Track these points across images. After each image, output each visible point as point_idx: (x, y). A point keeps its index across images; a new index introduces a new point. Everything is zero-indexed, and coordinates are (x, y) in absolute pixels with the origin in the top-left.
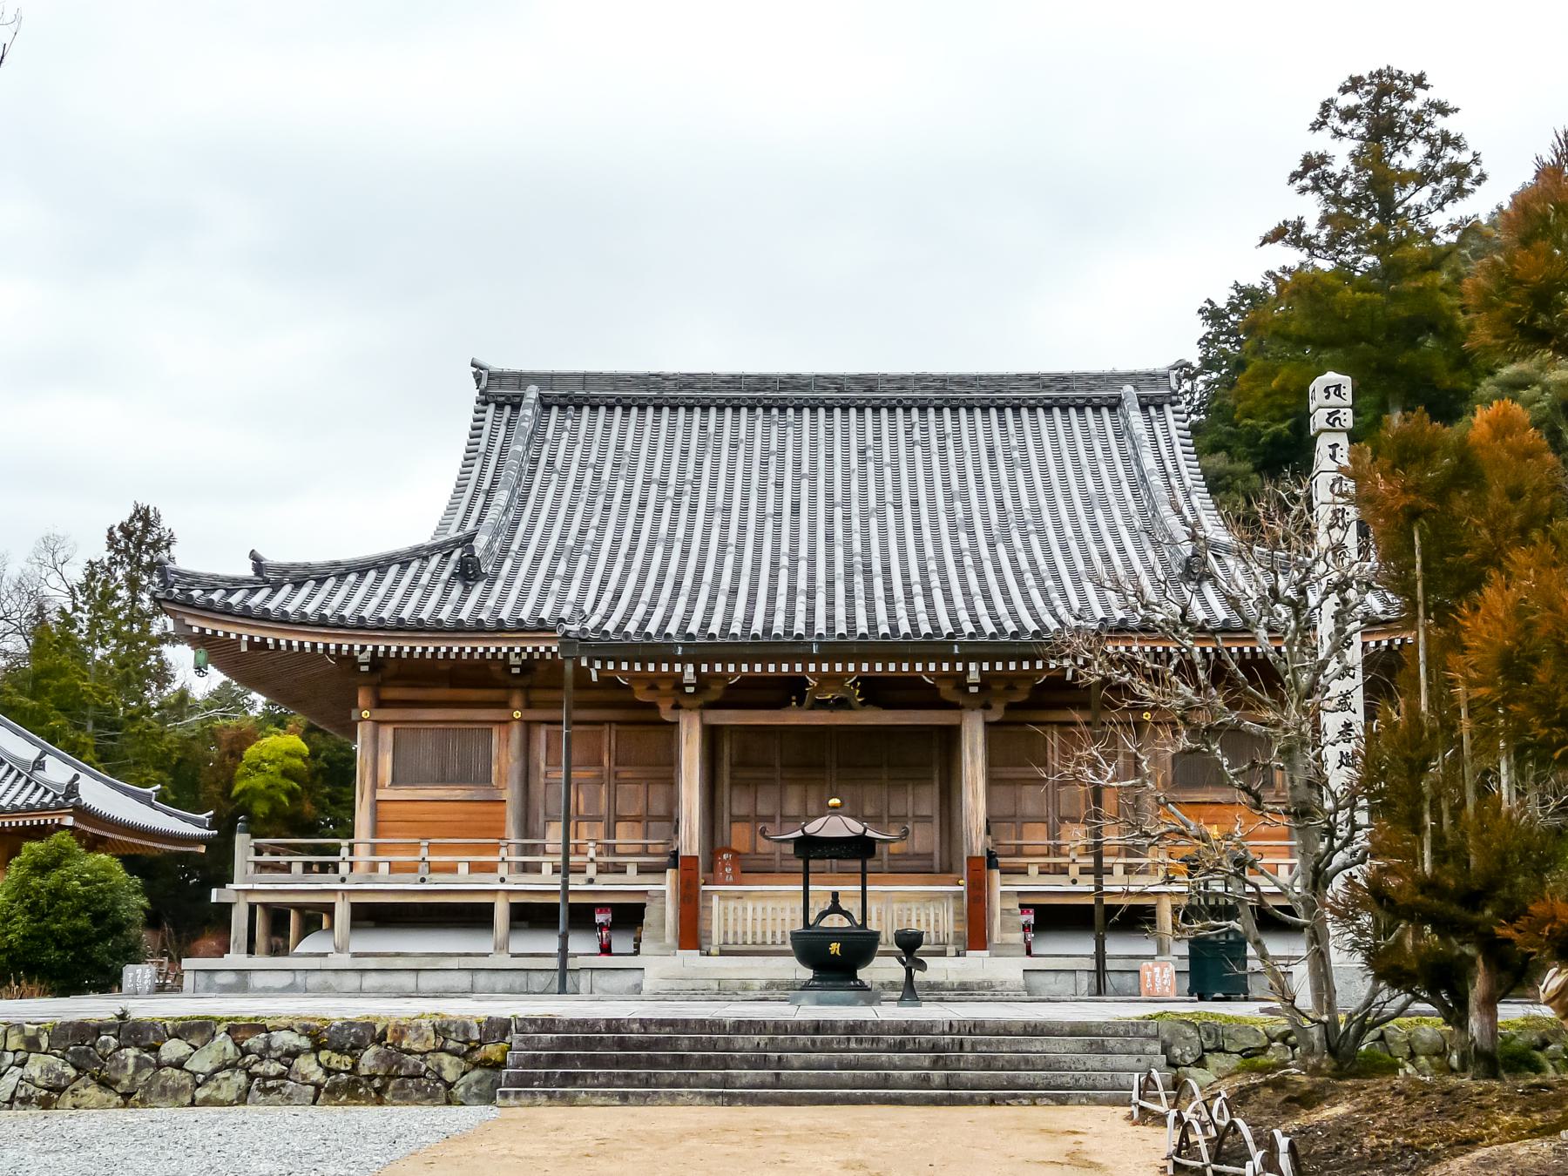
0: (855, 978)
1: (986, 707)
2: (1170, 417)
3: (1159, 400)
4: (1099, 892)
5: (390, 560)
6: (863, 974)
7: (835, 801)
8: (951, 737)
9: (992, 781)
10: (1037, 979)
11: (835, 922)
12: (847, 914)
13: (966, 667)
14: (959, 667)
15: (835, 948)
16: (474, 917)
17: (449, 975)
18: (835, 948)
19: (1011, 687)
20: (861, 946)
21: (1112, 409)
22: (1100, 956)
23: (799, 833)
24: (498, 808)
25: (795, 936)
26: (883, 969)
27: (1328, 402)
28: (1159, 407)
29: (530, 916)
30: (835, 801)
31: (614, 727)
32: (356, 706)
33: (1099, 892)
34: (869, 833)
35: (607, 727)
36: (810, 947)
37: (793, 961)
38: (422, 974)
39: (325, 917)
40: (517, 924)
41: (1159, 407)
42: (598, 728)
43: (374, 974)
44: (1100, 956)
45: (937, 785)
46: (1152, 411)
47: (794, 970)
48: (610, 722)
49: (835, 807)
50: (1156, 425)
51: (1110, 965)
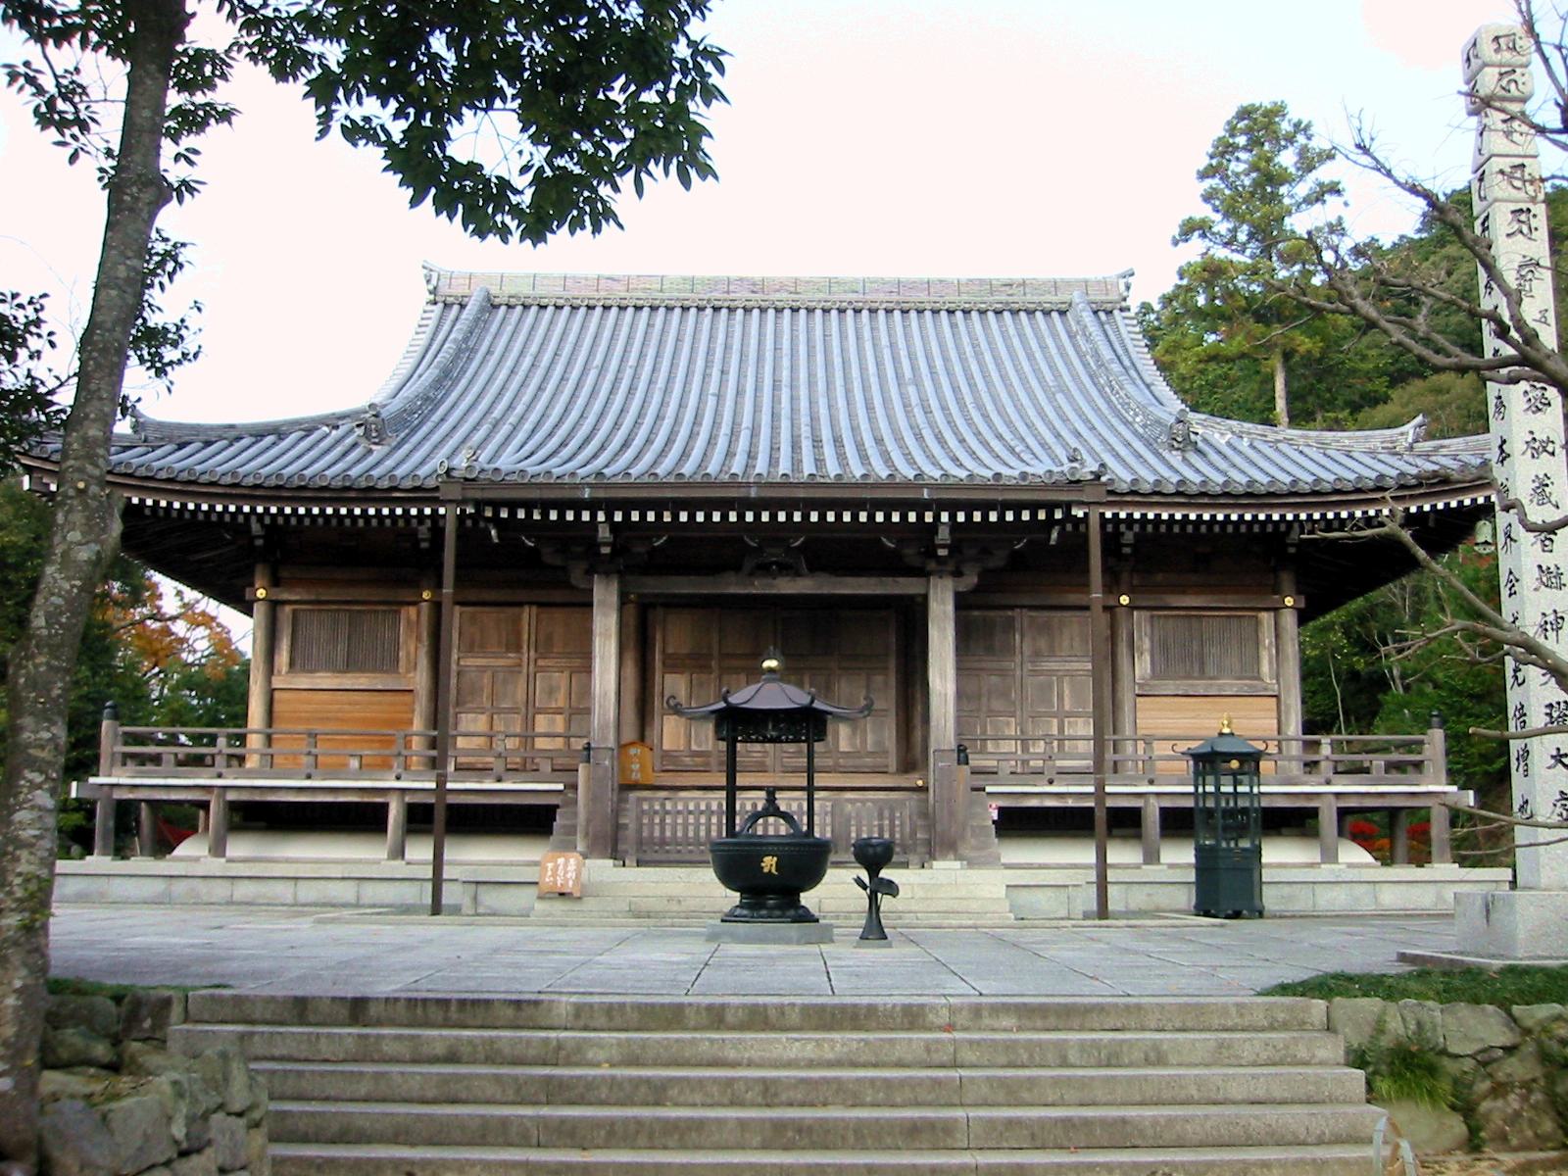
0: (795, 902)
1: (957, 574)
2: (1120, 322)
3: (1109, 307)
4: (1100, 794)
5: (295, 424)
6: (807, 899)
7: (771, 663)
8: (912, 620)
9: (961, 669)
10: (1024, 897)
11: (775, 827)
12: (787, 817)
13: (937, 517)
14: (929, 517)
15: (769, 863)
16: (359, 818)
17: (331, 885)
18: (769, 863)
19: (986, 551)
20: (807, 861)
21: (1062, 313)
22: (1102, 865)
23: (722, 705)
24: (407, 698)
25: (716, 848)
26: (837, 890)
27: (1497, 58)
28: (1109, 313)
29: (419, 818)
30: (771, 663)
31: (534, 609)
32: (252, 585)
33: (1100, 794)
34: (817, 705)
35: (527, 609)
36: (737, 864)
37: (708, 875)
38: (301, 883)
39: (202, 813)
40: (413, 826)
41: (1109, 313)
42: (516, 610)
43: (246, 882)
44: (1102, 865)
45: (892, 664)
46: (1102, 315)
47: (717, 894)
48: (531, 604)
49: (771, 670)
50: (1107, 327)
51: (1111, 875)
